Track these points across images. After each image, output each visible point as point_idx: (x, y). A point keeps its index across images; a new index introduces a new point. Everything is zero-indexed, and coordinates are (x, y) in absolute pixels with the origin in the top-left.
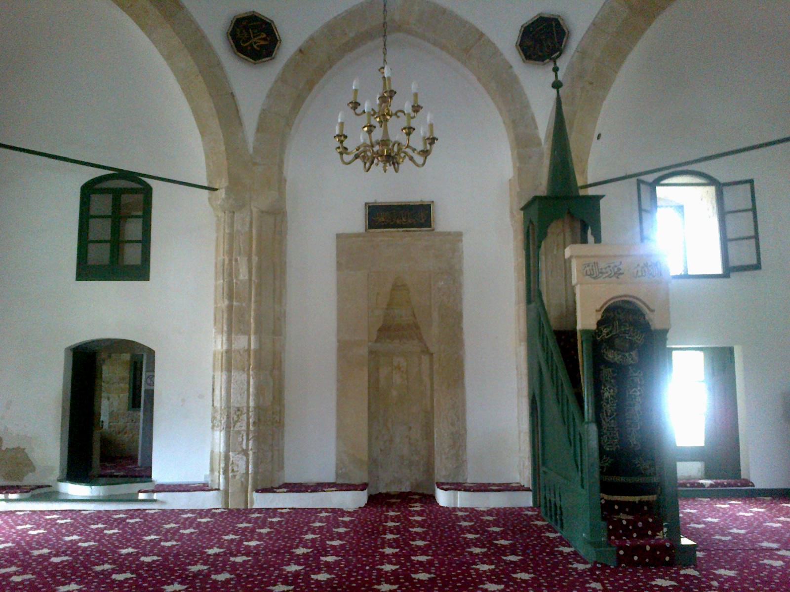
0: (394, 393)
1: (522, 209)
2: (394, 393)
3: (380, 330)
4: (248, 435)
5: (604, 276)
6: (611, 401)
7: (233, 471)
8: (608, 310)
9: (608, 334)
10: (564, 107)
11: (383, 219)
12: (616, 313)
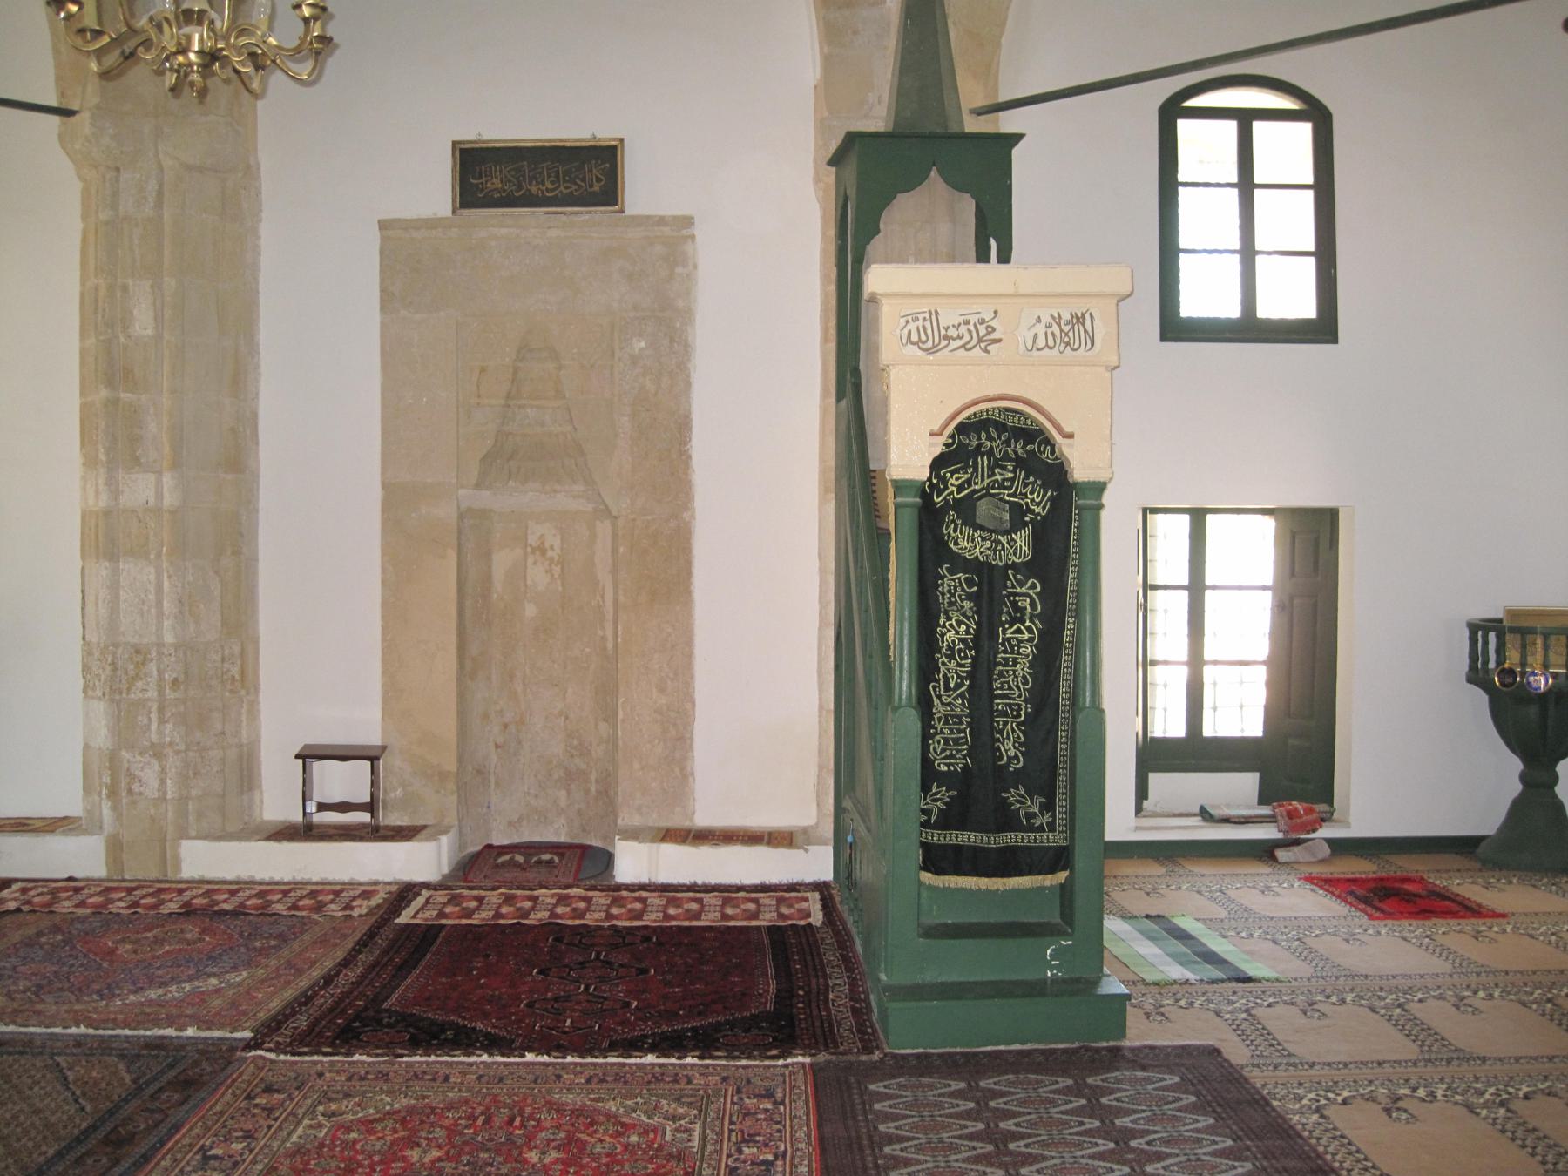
1: (831, 163)
2: (530, 610)
3: (488, 460)
4: (161, 710)
5: (954, 344)
7: (130, 791)
8: (962, 428)
9: (960, 488)
12: (983, 436)
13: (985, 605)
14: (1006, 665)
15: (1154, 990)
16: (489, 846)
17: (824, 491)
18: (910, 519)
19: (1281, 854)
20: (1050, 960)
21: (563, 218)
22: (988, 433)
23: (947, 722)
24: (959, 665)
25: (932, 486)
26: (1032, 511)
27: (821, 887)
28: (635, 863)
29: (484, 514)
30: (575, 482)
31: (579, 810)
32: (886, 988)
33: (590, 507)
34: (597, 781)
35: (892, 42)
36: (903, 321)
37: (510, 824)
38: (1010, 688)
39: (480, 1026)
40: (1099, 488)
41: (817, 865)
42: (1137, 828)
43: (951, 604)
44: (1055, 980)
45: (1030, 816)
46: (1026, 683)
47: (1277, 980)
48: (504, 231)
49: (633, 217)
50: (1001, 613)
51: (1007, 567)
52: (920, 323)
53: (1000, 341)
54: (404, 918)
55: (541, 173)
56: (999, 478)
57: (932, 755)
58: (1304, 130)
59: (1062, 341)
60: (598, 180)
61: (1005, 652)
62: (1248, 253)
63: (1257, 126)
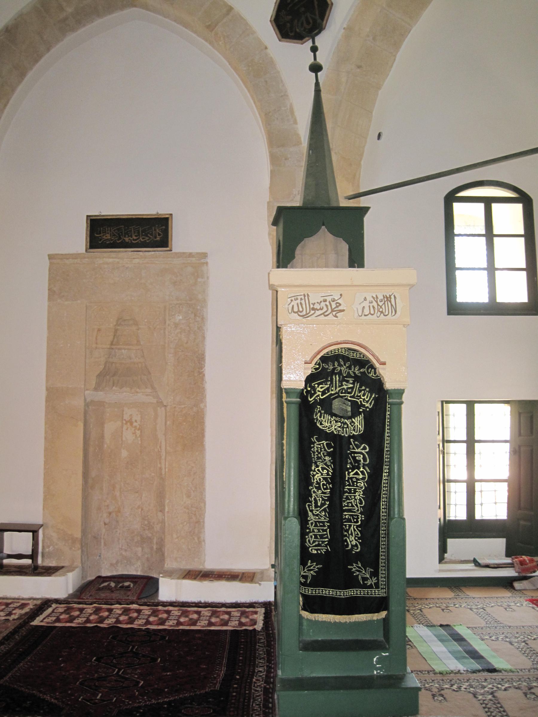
0: (124, 454)
2: (124, 454)
3: (101, 376)
6: (323, 485)
8: (324, 359)
9: (323, 393)
10: (324, 96)
11: (108, 236)
12: (336, 364)
13: (338, 460)
14: (350, 493)
15: (439, 677)
16: (99, 577)
17: (272, 393)
18: (295, 410)
19: (517, 585)
20: (376, 664)
21: (141, 253)
22: (339, 362)
23: (316, 526)
24: (323, 493)
25: (308, 392)
26: (364, 406)
27: (266, 605)
28: (169, 590)
29: (101, 404)
30: (146, 388)
31: (148, 558)
32: (283, 681)
33: (155, 401)
34: (157, 543)
35: (303, 163)
36: (289, 300)
37: (112, 565)
38: (352, 506)
39: (48, 698)
40: (400, 393)
41: (264, 592)
42: (441, 571)
43: (319, 458)
44: (379, 677)
45: (365, 579)
46: (361, 503)
47: (511, 671)
48: (111, 260)
49: (176, 253)
50: (347, 463)
51: (350, 437)
52: (299, 301)
53: (343, 311)
54: (36, 622)
55: (131, 231)
56: (345, 387)
57: (307, 544)
58: (519, 207)
59: (378, 311)
60: (159, 235)
61: (349, 485)
62: (491, 269)
63: (494, 206)
